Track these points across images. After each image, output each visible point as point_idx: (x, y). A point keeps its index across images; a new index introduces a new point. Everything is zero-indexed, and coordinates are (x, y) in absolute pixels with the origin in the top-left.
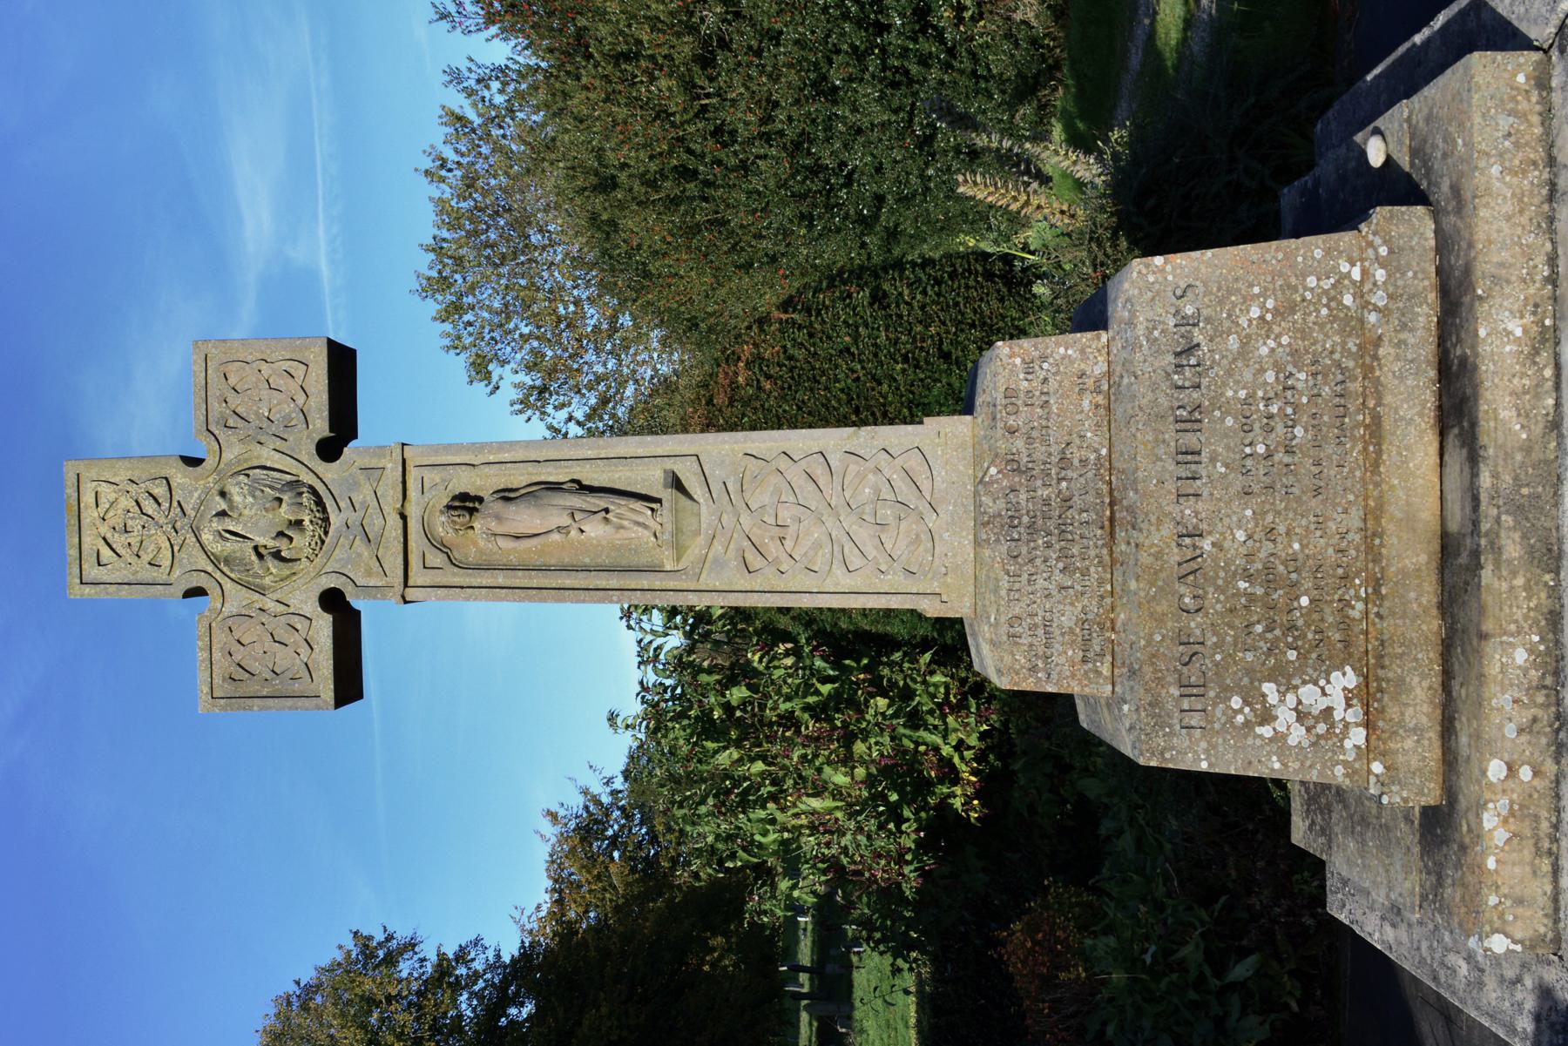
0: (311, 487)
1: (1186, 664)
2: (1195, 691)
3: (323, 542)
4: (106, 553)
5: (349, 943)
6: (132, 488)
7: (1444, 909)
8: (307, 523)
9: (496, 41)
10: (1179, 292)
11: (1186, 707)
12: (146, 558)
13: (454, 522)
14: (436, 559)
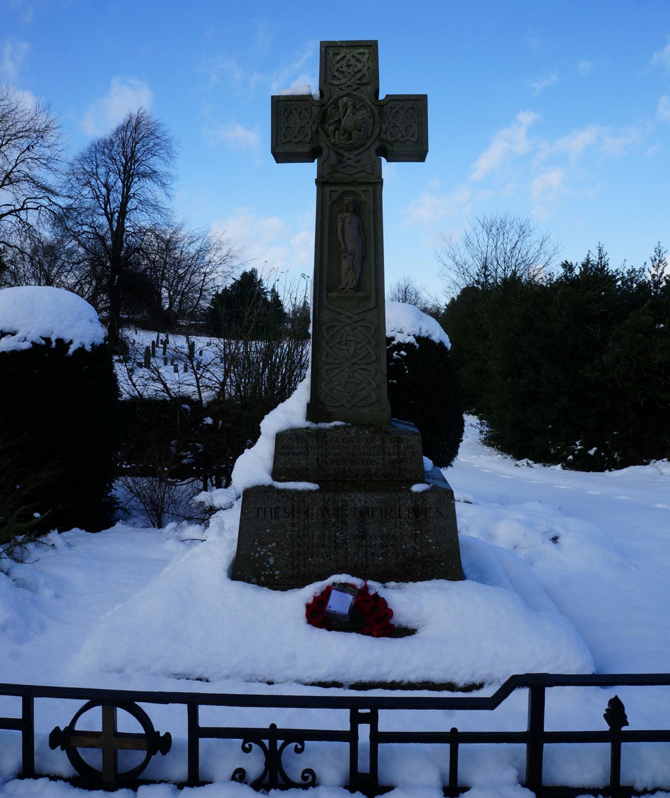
0: (365, 144)
1: (284, 510)
2: (273, 514)
3: (342, 148)
4: (339, 57)
5: (453, 464)
6: (366, 69)
7: (173, 157)
8: (350, 142)
9: (657, 245)
10: (439, 510)
11: (267, 510)
12: (336, 74)
13: (349, 204)
14: (335, 196)
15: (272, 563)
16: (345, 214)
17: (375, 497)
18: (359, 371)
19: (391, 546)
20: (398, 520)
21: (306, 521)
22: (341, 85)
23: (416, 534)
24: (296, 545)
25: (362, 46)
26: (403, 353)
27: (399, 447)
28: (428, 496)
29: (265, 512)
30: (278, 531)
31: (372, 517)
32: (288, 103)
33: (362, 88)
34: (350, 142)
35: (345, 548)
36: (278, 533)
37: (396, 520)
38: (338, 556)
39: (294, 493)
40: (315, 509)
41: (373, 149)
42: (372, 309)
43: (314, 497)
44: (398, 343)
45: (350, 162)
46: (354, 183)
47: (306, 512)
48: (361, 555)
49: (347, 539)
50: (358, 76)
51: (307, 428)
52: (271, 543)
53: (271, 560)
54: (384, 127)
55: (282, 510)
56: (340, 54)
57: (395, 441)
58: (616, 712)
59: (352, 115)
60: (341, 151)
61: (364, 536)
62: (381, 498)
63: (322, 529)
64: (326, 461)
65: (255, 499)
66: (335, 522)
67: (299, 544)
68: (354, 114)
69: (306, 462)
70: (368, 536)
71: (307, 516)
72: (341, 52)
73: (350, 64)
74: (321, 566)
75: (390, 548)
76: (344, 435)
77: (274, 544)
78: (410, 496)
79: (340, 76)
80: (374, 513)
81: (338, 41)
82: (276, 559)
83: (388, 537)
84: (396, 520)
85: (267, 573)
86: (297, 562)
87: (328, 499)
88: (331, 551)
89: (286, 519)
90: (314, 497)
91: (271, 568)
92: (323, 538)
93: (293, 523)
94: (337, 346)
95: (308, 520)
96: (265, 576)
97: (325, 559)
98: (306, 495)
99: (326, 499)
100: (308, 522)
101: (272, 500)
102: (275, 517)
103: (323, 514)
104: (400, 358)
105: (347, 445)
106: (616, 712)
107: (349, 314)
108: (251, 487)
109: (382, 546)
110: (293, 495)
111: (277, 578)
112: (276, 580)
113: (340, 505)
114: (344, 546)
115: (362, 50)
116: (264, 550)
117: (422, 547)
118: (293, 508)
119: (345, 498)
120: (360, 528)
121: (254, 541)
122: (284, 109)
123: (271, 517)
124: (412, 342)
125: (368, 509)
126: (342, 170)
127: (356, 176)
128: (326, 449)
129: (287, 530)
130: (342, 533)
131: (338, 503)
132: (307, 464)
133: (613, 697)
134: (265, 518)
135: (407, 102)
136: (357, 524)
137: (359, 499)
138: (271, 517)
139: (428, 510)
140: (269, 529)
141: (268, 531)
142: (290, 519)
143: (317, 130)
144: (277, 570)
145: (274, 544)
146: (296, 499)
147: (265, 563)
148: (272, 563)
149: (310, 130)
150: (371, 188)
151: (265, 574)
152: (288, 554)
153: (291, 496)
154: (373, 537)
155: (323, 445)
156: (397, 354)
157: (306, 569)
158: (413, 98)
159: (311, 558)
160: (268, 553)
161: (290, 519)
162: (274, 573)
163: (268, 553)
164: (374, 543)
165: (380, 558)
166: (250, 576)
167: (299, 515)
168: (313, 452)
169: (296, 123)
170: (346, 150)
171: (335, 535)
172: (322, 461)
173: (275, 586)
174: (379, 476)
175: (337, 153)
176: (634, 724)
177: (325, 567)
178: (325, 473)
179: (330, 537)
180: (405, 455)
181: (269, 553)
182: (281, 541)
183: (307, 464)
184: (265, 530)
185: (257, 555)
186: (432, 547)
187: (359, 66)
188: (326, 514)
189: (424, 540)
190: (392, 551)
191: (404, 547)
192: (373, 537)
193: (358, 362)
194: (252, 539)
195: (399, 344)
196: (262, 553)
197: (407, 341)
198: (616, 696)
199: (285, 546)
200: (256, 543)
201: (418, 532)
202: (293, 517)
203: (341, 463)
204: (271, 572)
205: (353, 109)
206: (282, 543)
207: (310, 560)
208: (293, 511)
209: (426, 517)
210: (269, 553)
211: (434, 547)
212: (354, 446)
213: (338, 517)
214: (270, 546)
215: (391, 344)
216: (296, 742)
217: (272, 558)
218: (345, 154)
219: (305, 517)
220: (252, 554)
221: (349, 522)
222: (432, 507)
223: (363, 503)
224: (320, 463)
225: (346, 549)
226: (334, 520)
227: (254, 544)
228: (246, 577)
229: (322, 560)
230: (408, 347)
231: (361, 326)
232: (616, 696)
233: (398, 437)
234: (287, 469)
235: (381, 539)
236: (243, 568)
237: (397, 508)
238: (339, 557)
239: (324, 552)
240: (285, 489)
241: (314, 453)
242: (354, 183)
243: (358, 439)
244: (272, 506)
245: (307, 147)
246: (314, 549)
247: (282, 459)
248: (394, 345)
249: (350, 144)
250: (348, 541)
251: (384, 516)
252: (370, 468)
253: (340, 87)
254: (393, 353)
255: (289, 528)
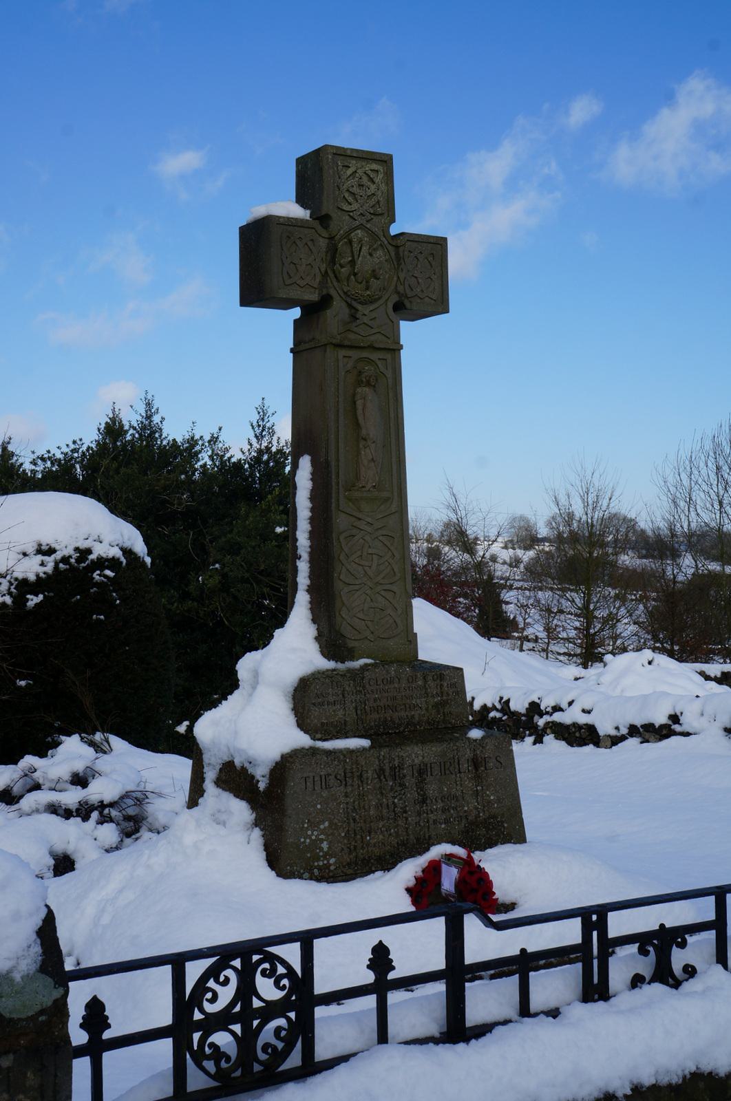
1: (336, 777)
2: (323, 784)
3: (355, 300)
8: (368, 293)
12: (347, 195)
15: (325, 849)
16: (365, 389)
17: (433, 749)
18: (383, 593)
19: (453, 808)
20: (458, 775)
21: (361, 788)
22: (352, 211)
23: (477, 790)
24: (352, 821)
25: (375, 160)
26: (108, 572)
27: (442, 685)
28: (487, 743)
29: (314, 781)
30: (330, 806)
31: (431, 775)
32: (290, 228)
33: (376, 219)
34: (368, 293)
35: (405, 817)
36: (330, 808)
37: (456, 775)
38: (398, 830)
39: (345, 753)
40: (369, 771)
41: (390, 305)
42: (394, 513)
43: (368, 755)
44: (97, 558)
45: (365, 320)
46: (372, 348)
47: (361, 776)
48: (422, 824)
49: (406, 806)
50: (373, 201)
51: (334, 670)
52: (323, 822)
53: (325, 846)
54: (402, 276)
55: (333, 777)
56: (349, 167)
57: (437, 678)
58: (380, 958)
59: (368, 257)
60: (355, 304)
61: (424, 800)
62: (439, 750)
63: (379, 796)
64: (365, 709)
65: (302, 767)
66: (392, 786)
67: (354, 820)
68: (371, 255)
69: (344, 713)
70: (428, 799)
71: (362, 782)
72: (351, 165)
73: (362, 183)
74: (380, 844)
75: (452, 811)
76: (383, 675)
77: (327, 824)
78: (468, 744)
79: (350, 199)
80: (433, 769)
81: (347, 149)
82: (330, 843)
83: (449, 799)
84: (456, 775)
85: (321, 863)
86: (353, 843)
87: (383, 756)
88: (390, 823)
89: (338, 788)
90: (368, 755)
91: (324, 857)
92: (380, 808)
93: (346, 792)
94: (357, 561)
95: (363, 786)
96: (320, 868)
97: (384, 836)
98: (359, 754)
99: (381, 757)
100: (363, 789)
101: (321, 764)
102: (326, 788)
103: (379, 777)
104: (105, 580)
105: (387, 688)
106: (380, 958)
107: (369, 520)
108: (289, 751)
109: (444, 810)
110: (345, 756)
111: (332, 868)
112: (332, 871)
113: (396, 763)
114: (404, 815)
115: (374, 166)
116: (316, 833)
117: (484, 807)
118: (345, 774)
119: (401, 754)
120: (419, 790)
121: (303, 823)
122: (258, 239)
123: (322, 788)
124: (117, 556)
125: (427, 765)
126: (355, 329)
127: (372, 338)
128: (365, 695)
129: (339, 804)
130: (401, 799)
131: (394, 761)
132: (345, 715)
133: (377, 942)
134: (314, 789)
135: (425, 244)
136: (416, 785)
137: (415, 754)
138: (322, 788)
139: (487, 760)
140: (320, 804)
141: (319, 806)
142: (342, 788)
143: (326, 272)
144: (332, 857)
145: (327, 824)
146: (348, 761)
147: (318, 851)
148: (325, 849)
149: (318, 271)
150: (388, 356)
151: (318, 865)
152: (343, 834)
153: (342, 757)
154: (434, 800)
155: (361, 689)
156: (100, 575)
157: (365, 851)
158: (432, 241)
159: (370, 836)
160: (320, 837)
161: (342, 788)
162: (328, 861)
163: (320, 837)
164: (435, 807)
165: (443, 826)
166: (302, 871)
167: (353, 781)
168: (350, 700)
169: (301, 259)
170: (360, 303)
171: (394, 802)
172: (361, 710)
173: (332, 879)
174: (424, 724)
175: (350, 306)
176: (402, 967)
177: (385, 845)
178: (365, 725)
179: (388, 805)
180: (448, 695)
181: (322, 837)
182: (335, 818)
183: (345, 715)
184: (315, 806)
185: (308, 841)
186: (494, 804)
187: (373, 187)
188: (382, 777)
189: (485, 798)
190: (454, 815)
191: (466, 808)
192: (434, 800)
193: (382, 582)
194: (301, 821)
195: (100, 559)
196: (313, 837)
197: (110, 556)
198: (381, 942)
199: (339, 824)
200: (306, 825)
201: (478, 788)
202: (346, 785)
203: (382, 710)
204: (325, 862)
205: (369, 249)
206: (336, 821)
207: (368, 838)
208: (345, 777)
209: (486, 769)
210: (322, 837)
211: (496, 805)
212: (395, 688)
213: (395, 780)
214: (322, 827)
215: (87, 559)
216: (235, 1061)
217: (325, 842)
218: (359, 307)
219: (360, 783)
220: (302, 840)
221: (407, 784)
222: (491, 756)
223: (421, 758)
224: (359, 712)
225: (407, 819)
226: (391, 783)
227: (303, 827)
228: (296, 873)
229: (381, 837)
230: (112, 563)
231: (383, 535)
232: (381, 942)
233: (440, 674)
234: (323, 724)
235: (442, 801)
236: (292, 861)
237: (456, 761)
238: (400, 830)
239: (383, 826)
240: (334, 749)
241: (352, 701)
242: (372, 348)
243: (399, 680)
244: (322, 773)
245: (315, 293)
246: (372, 824)
247: (315, 711)
248: (92, 561)
249: (368, 295)
250: (408, 808)
251: (443, 774)
252: (414, 715)
253: (351, 214)
254: (92, 574)
255: (342, 799)
